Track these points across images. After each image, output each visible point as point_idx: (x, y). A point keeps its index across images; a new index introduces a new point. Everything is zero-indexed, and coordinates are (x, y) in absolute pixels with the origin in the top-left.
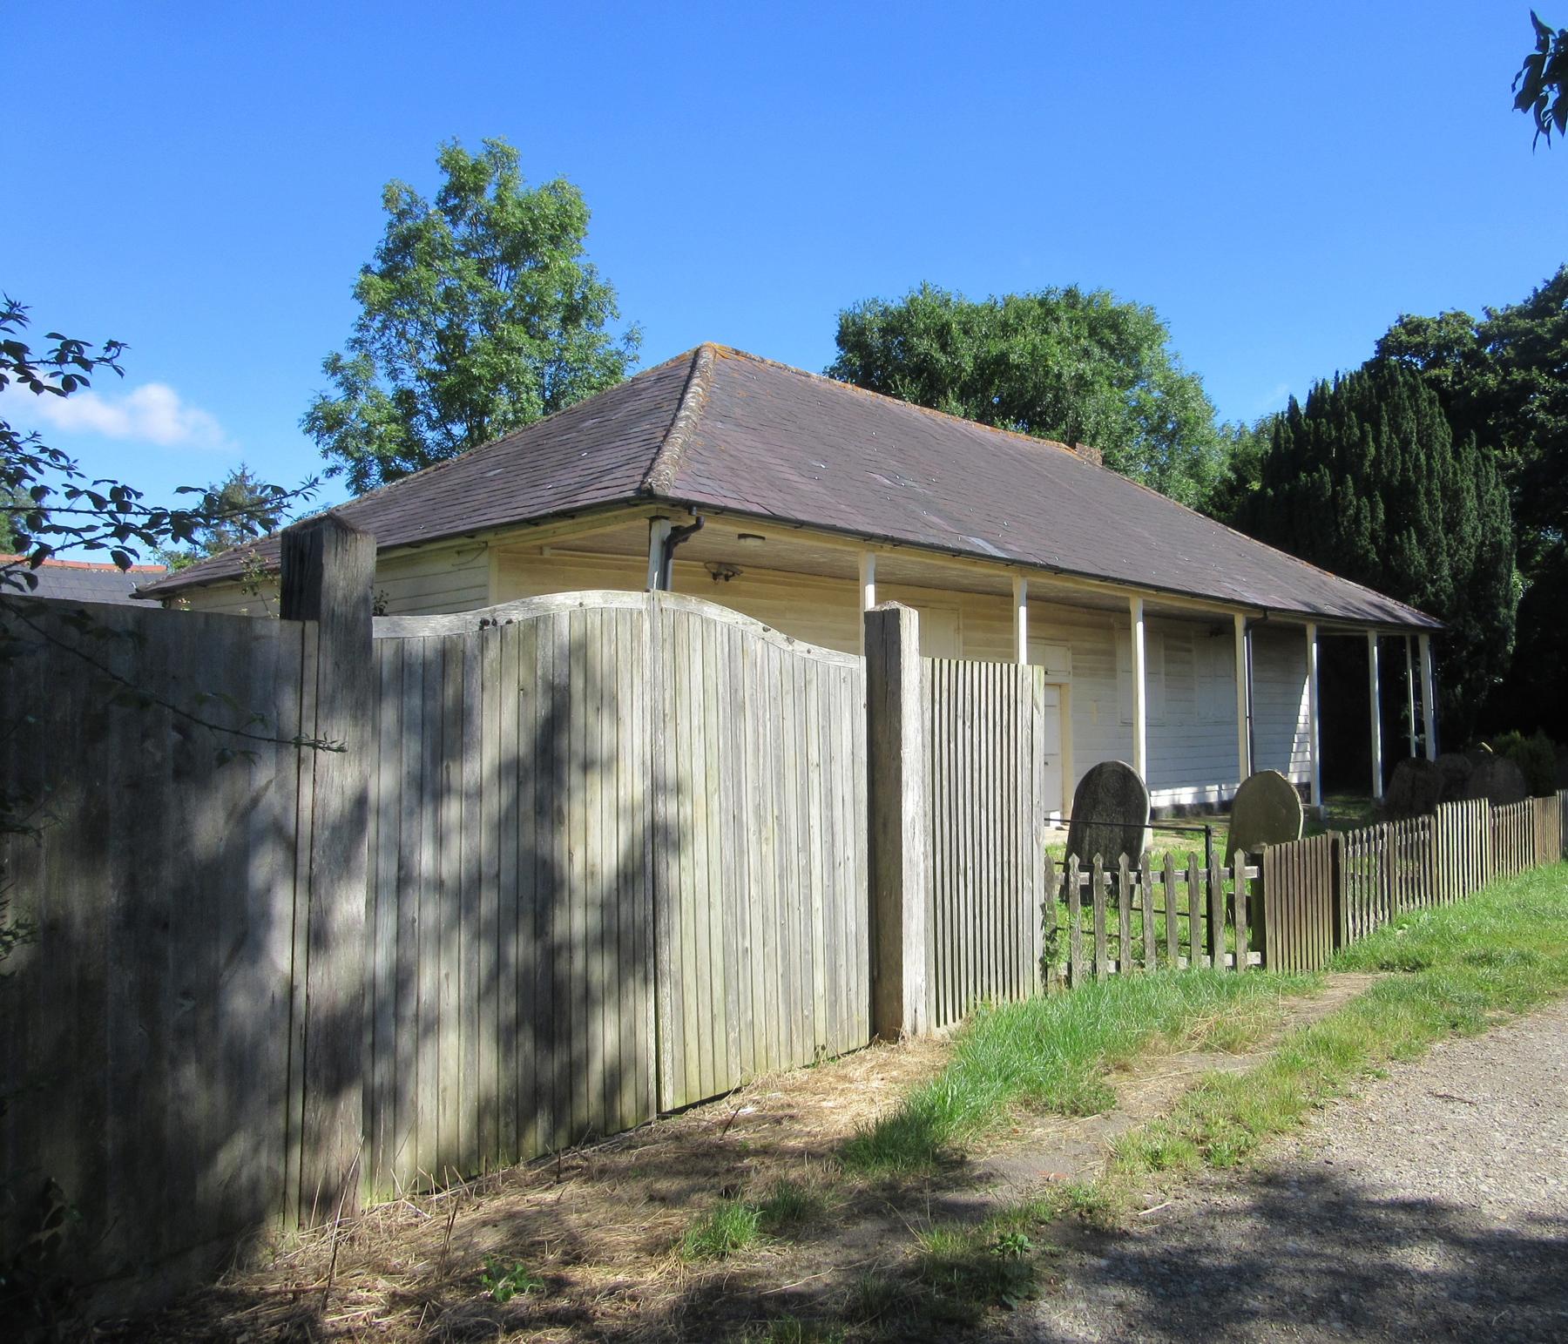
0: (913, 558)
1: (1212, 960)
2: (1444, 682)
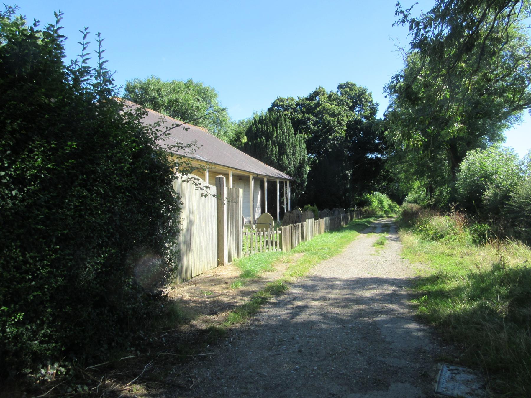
1: (282, 250)
2: (292, 191)
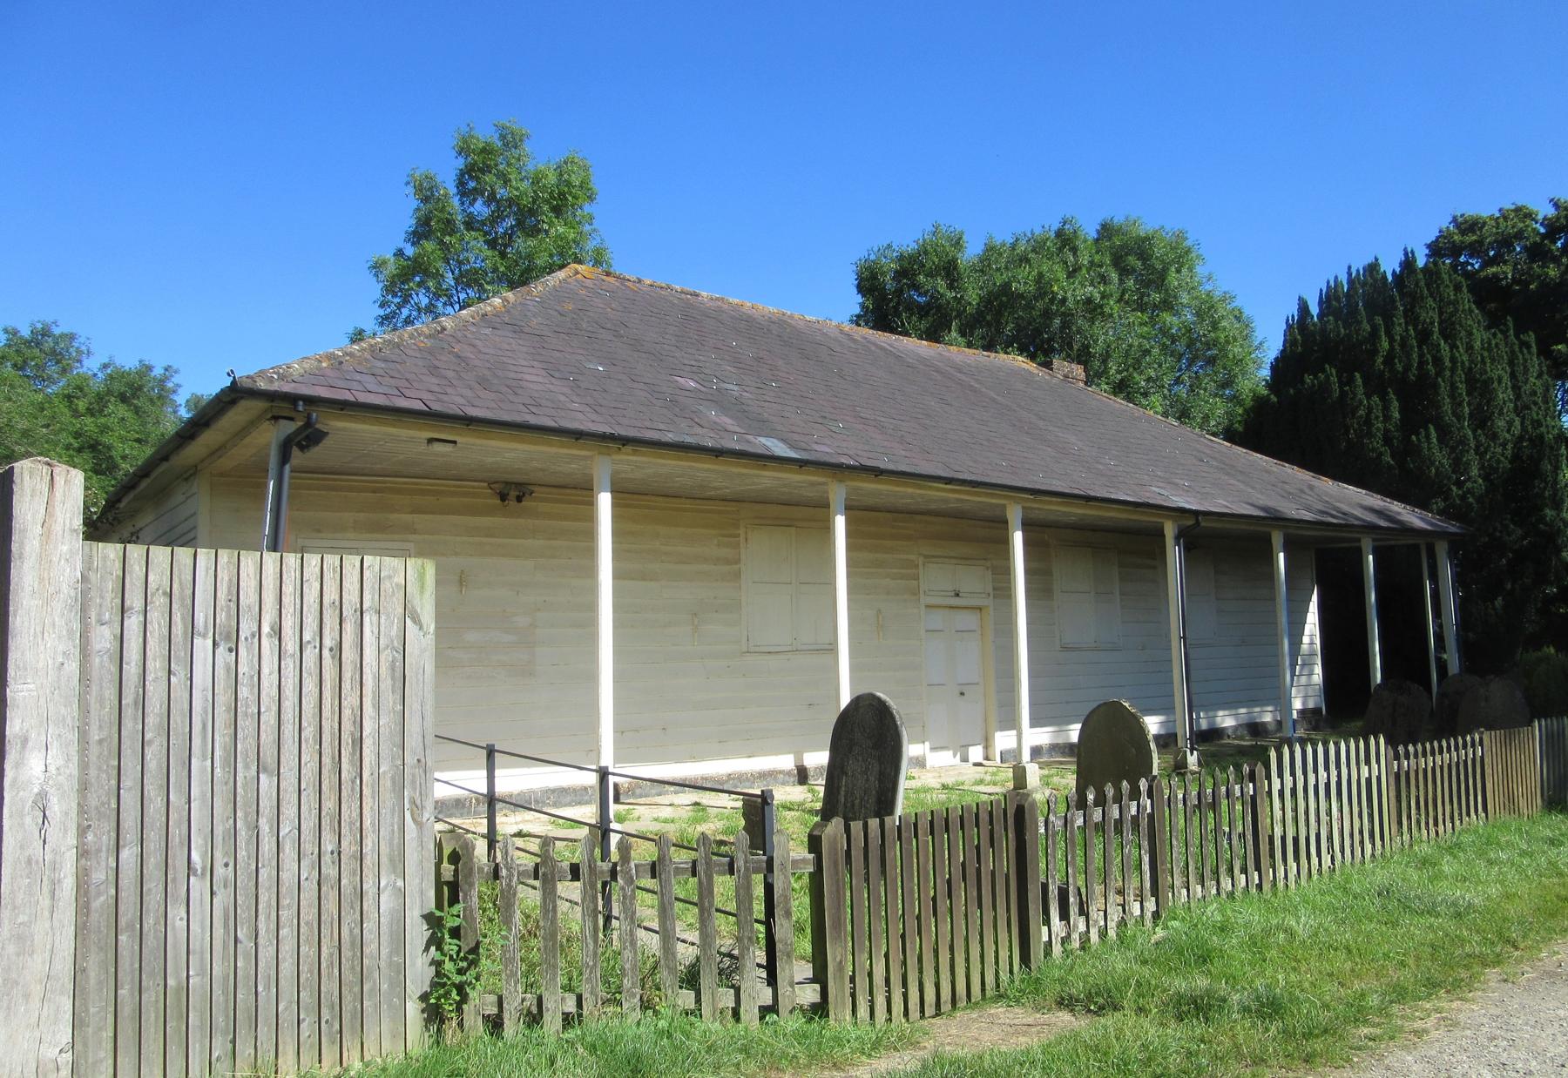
0: (706, 466)
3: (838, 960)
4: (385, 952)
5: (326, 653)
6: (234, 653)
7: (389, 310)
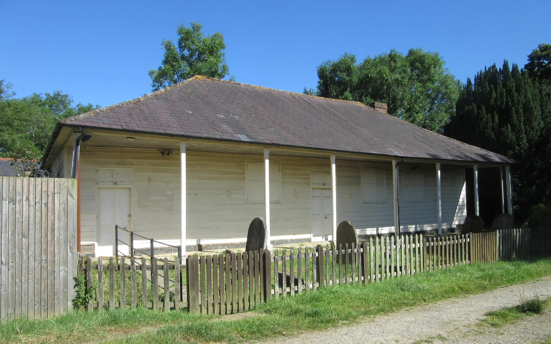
3: (193, 295)
4: (61, 288)
5: (43, 205)
6: (15, 205)
7: (155, 88)
